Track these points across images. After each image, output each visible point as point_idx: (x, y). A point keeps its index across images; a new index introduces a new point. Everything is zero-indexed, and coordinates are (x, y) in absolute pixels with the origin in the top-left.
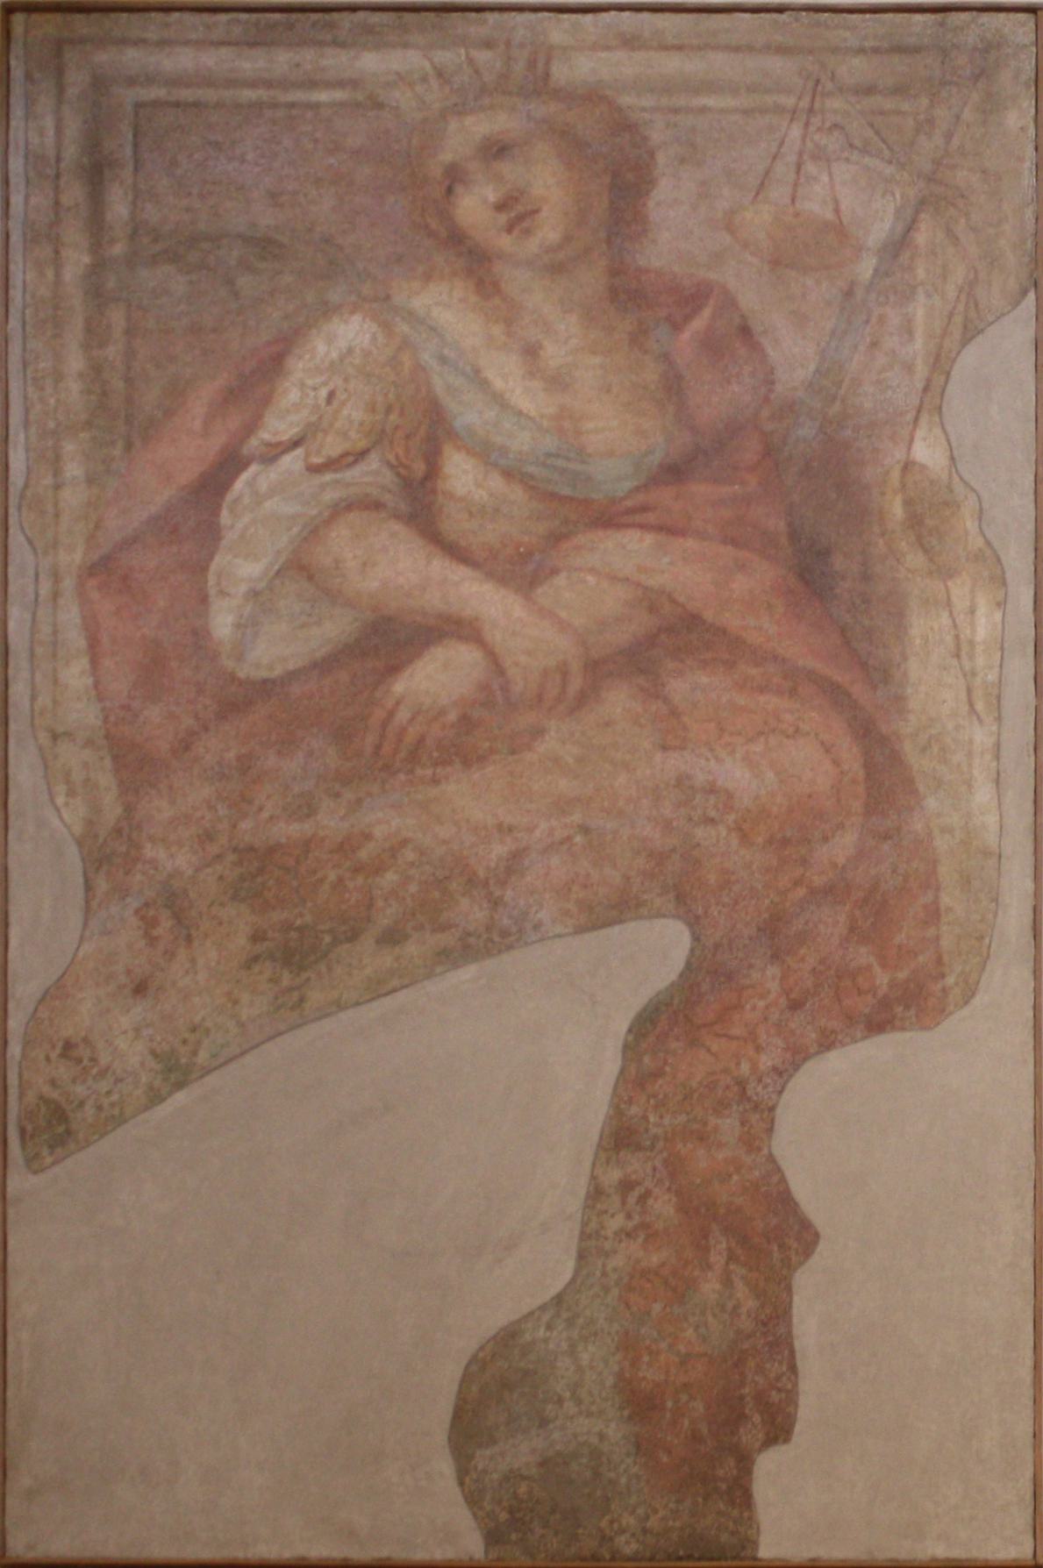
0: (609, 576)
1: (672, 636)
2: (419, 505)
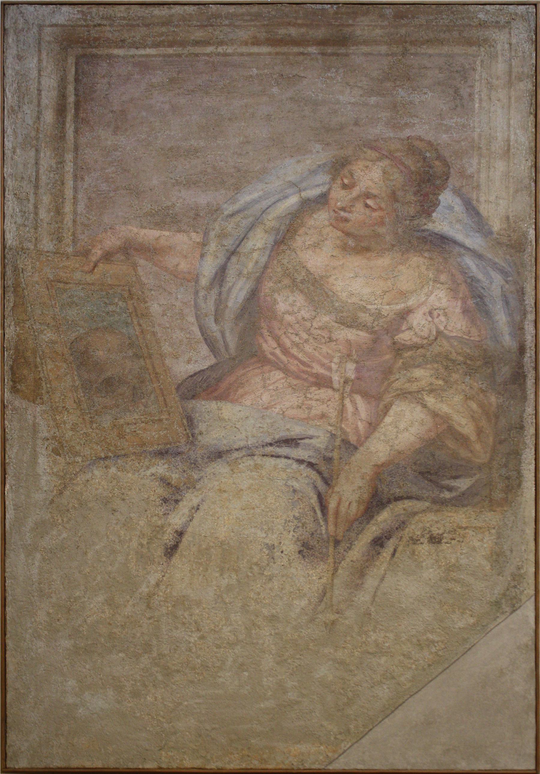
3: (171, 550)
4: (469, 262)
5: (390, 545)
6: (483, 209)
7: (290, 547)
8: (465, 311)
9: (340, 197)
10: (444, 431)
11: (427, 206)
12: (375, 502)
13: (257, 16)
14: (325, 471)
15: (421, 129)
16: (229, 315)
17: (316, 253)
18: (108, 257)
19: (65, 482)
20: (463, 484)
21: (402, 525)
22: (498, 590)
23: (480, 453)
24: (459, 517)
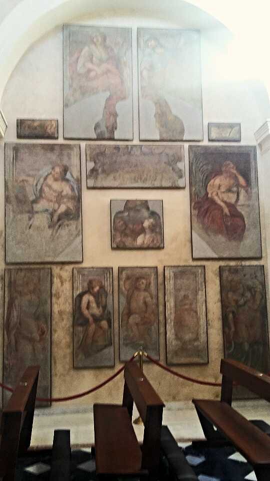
0: (104, 66)
1: (108, 71)
2: (91, 61)
3: (30, 228)
6: (73, 174)
7: (47, 226)
9: (53, 172)
10: (68, 208)
12: (59, 220)
14: (52, 215)
16: (38, 190)
17: (50, 181)
18: (21, 182)
19: (14, 216)
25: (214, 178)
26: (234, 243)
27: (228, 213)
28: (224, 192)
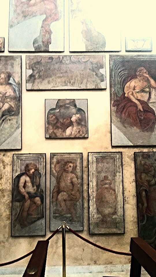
4: (13, 86)
5: (5, 121)
8: (13, 92)
10: (11, 106)
11: (9, 80)
13: (20, 96)
15: (9, 70)
20: (13, 113)
21: (6, 118)
22: (17, 126)
23: (15, 109)
24: (13, 117)
25: (130, 80)
26: (147, 134)
27: (142, 110)
28: (138, 92)
